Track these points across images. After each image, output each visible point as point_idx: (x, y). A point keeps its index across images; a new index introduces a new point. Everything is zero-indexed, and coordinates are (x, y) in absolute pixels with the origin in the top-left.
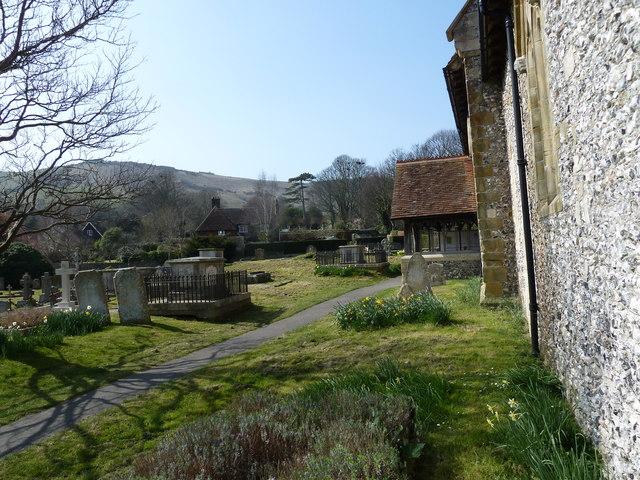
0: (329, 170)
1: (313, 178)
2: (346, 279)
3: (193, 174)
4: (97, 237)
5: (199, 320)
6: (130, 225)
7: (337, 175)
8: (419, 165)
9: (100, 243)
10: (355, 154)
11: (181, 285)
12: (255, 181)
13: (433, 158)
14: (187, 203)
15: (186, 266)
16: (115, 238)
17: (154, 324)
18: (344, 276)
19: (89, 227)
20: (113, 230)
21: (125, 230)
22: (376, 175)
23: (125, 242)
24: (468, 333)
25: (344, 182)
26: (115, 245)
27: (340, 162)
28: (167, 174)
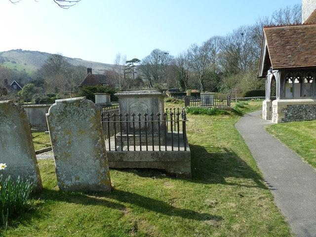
0: (149, 57)
1: (139, 61)
2: (213, 117)
3: (71, 59)
4: (19, 89)
5: (173, 176)
6: (39, 82)
7: (152, 61)
8: (283, 30)
9: (21, 92)
10: (163, 49)
11: (137, 125)
12: (112, 65)
13: (291, 25)
14: (71, 71)
15: (140, 99)
16: (30, 90)
17: (125, 197)
18: (210, 115)
19: (14, 83)
20: (29, 85)
21: (35, 86)
22: (174, 61)
23: (36, 92)
24: (3, 216)
25: (156, 66)
26: (30, 94)
27: (155, 53)
28: (59, 57)
